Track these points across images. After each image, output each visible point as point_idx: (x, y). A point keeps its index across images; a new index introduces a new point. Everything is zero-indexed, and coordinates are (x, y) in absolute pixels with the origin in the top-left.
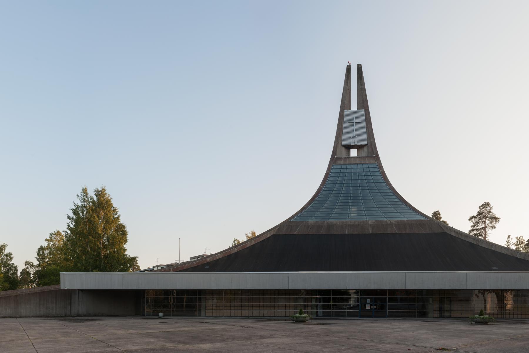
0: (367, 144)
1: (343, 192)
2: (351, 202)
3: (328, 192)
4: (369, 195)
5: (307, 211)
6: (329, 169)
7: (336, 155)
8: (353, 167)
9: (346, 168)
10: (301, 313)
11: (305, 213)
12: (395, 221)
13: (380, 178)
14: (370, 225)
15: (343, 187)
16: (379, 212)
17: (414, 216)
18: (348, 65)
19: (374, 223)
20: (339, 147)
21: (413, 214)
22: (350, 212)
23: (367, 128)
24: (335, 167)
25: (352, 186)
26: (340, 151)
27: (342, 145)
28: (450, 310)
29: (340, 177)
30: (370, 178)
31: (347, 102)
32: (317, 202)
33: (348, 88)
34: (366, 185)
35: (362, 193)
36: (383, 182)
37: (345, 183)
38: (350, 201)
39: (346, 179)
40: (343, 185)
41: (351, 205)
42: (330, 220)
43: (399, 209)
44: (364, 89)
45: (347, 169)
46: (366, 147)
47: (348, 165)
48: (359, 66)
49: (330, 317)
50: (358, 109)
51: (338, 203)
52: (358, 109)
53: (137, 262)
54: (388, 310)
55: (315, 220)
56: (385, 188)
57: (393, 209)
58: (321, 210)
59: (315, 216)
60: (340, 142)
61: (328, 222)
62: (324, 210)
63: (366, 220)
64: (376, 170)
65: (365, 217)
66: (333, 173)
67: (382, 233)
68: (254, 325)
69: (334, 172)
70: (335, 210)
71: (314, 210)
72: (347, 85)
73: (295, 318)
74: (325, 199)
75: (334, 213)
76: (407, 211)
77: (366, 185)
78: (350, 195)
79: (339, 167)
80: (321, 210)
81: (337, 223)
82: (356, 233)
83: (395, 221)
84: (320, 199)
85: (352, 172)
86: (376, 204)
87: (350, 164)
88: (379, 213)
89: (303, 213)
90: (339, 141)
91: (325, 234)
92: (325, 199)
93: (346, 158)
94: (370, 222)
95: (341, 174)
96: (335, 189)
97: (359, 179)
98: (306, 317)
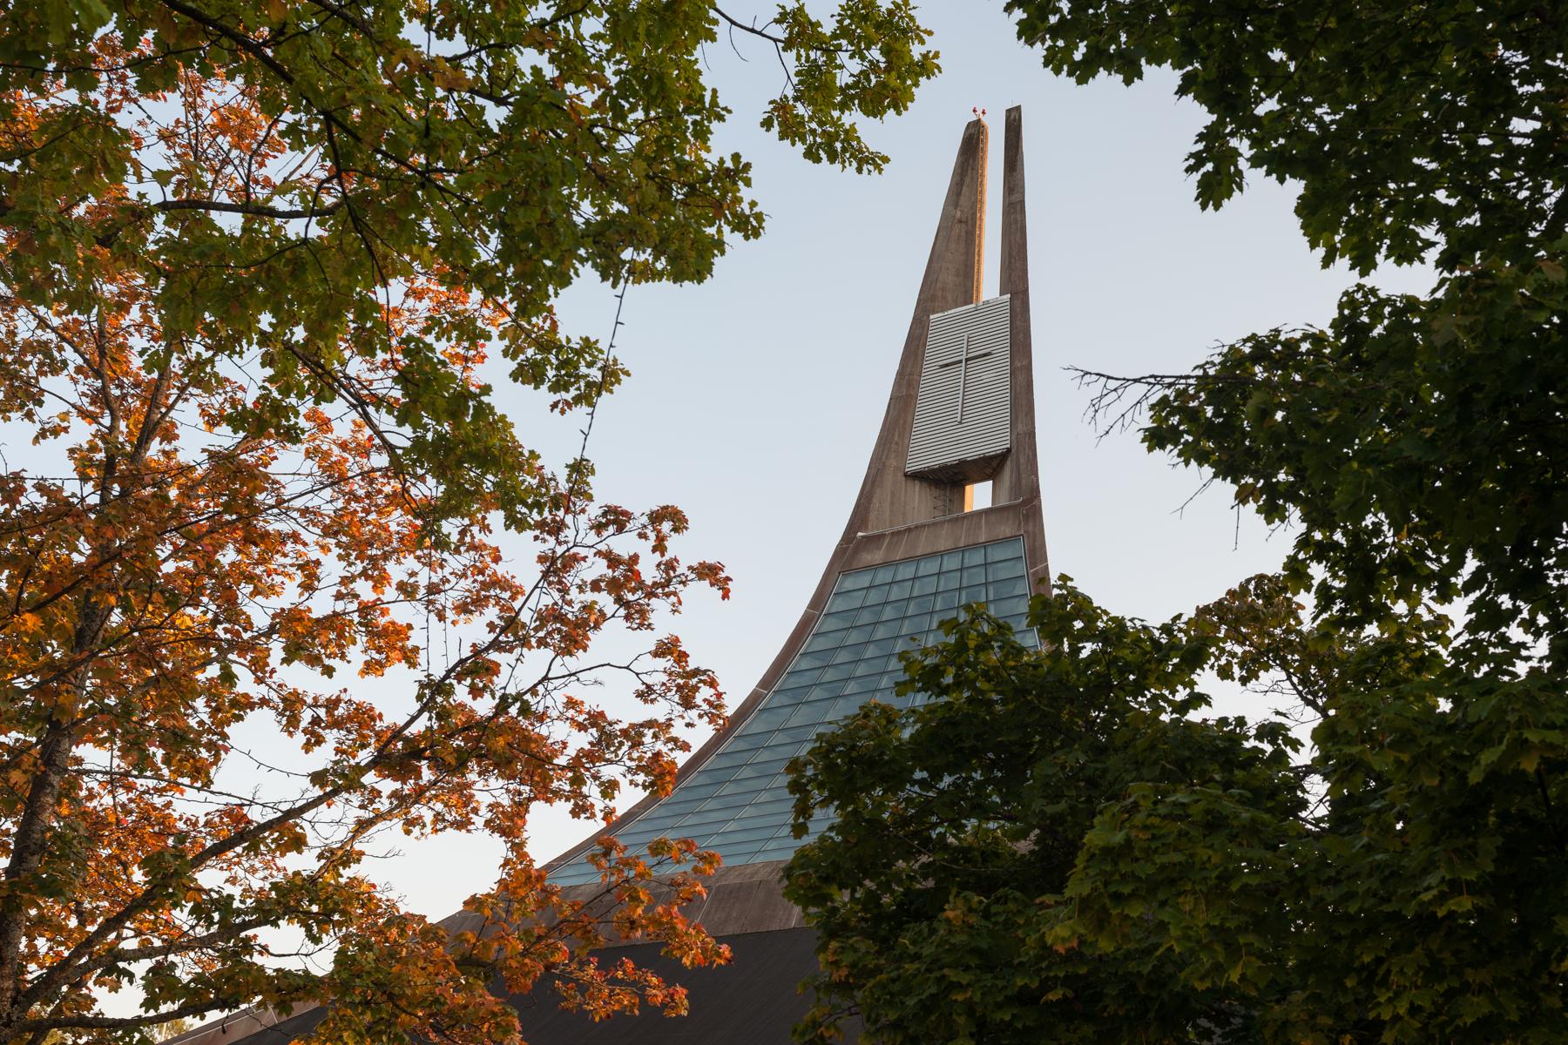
6: (818, 601)
24: (849, 584)
26: (892, 503)
27: (906, 475)
40: (966, 561)
53: (909, 104)
79: (865, 580)
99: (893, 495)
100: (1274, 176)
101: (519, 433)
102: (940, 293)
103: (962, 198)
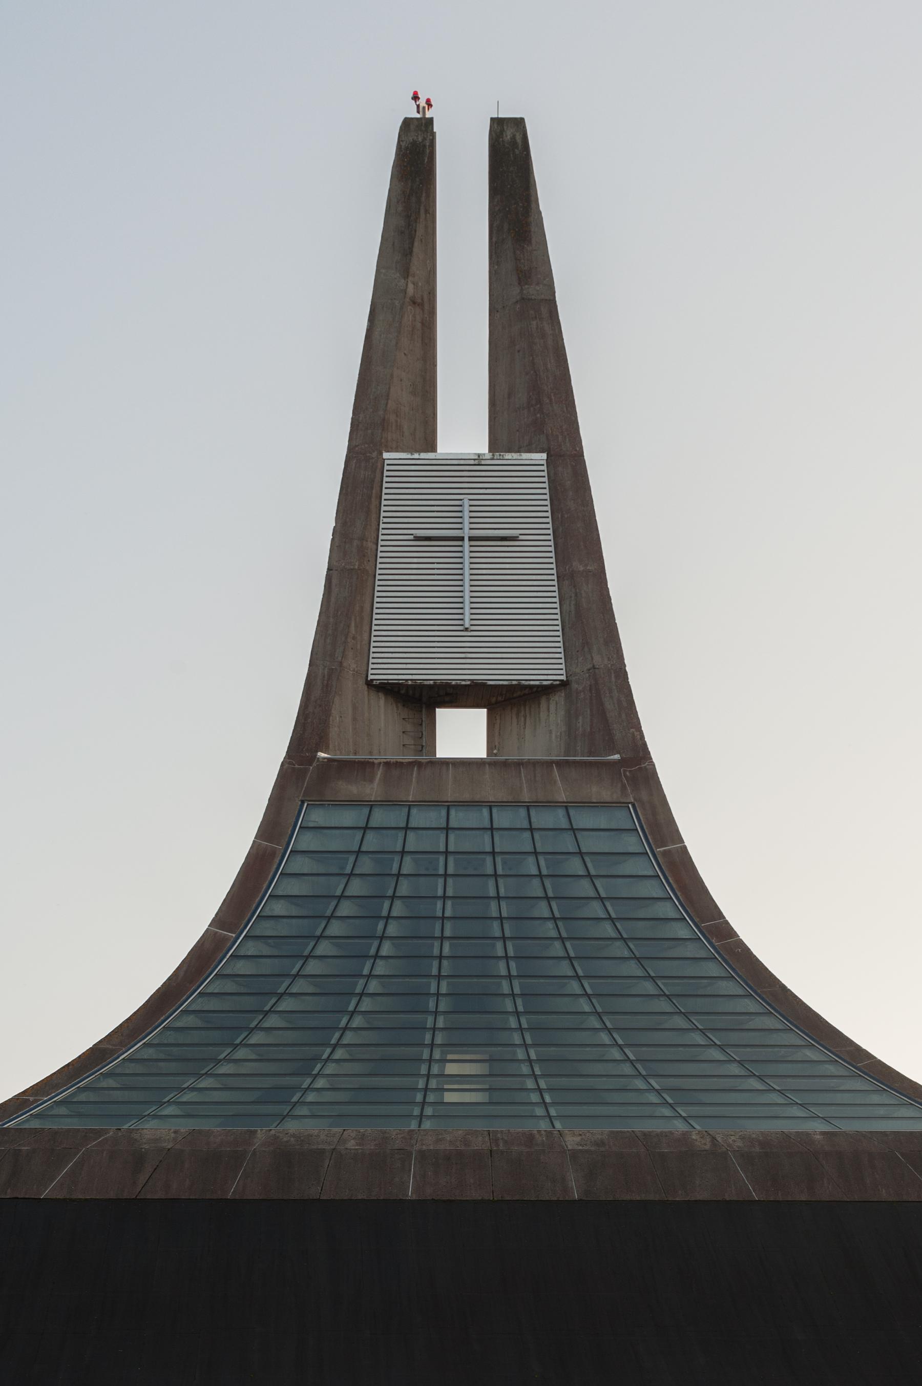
0: (564, 684)
3: (267, 966)
5: (118, 1071)
7: (323, 743)
8: (413, 824)
11: (111, 1083)
13: (657, 893)
14: (574, 1155)
16: (640, 1084)
17: (882, 1111)
18: (407, 123)
19: (601, 1143)
21: (876, 1098)
22: (437, 1055)
23: (565, 576)
24: (318, 817)
26: (354, 719)
27: (369, 684)
30: (584, 888)
33: (411, 289)
34: (549, 929)
35: (519, 976)
36: (672, 914)
37: (394, 913)
38: (437, 944)
41: (446, 951)
42: (292, 1126)
43: (783, 1069)
44: (544, 310)
46: (559, 699)
47: (414, 811)
48: (502, 131)
50: (494, 446)
51: (362, 994)
52: (491, 450)
55: (186, 1126)
56: (689, 955)
57: (735, 1069)
59: (184, 1099)
60: (351, 664)
63: (544, 1125)
64: (631, 843)
65: (540, 1111)
67: (651, 1197)
69: (312, 848)
72: (406, 273)
74: (248, 1002)
76: (833, 1083)
79: (349, 817)
83: (742, 1138)
84: (213, 1004)
86: (609, 1025)
88: (604, 1045)
89: (97, 1080)
91: (257, 1197)
92: (248, 1002)
93: (399, 765)
99: (355, 708)
102: (392, 418)
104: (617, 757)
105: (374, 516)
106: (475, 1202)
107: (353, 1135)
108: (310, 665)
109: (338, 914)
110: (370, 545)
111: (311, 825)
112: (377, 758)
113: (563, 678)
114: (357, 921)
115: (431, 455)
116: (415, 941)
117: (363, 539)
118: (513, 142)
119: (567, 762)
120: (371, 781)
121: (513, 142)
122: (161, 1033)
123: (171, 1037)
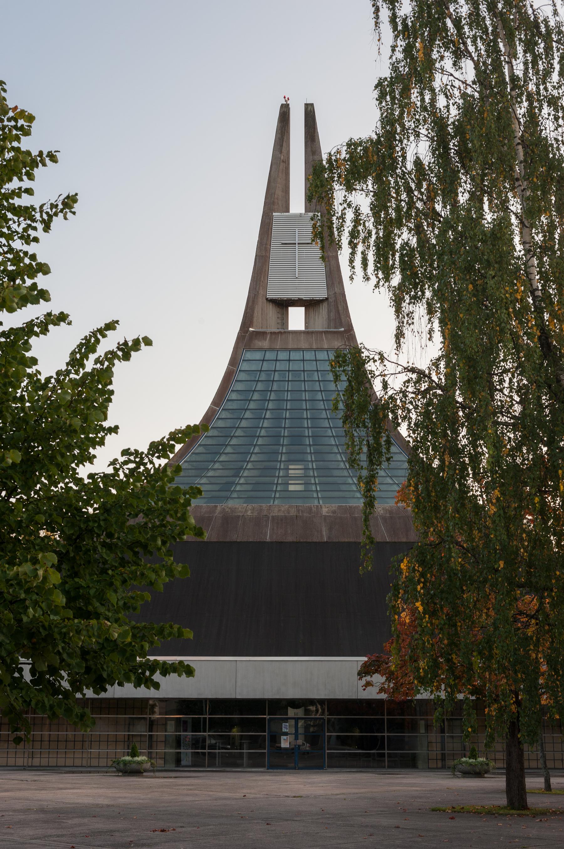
1: (265, 425)
2: (284, 451)
3: (229, 423)
4: (329, 433)
6: (234, 361)
7: (251, 325)
8: (291, 358)
9: (275, 359)
10: (134, 755)
12: (383, 509)
15: (267, 409)
18: (282, 105)
19: (334, 512)
20: (261, 302)
24: (249, 355)
25: (288, 407)
26: (262, 314)
27: (267, 299)
28: (131, 737)
29: (259, 384)
31: (279, 193)
32: (201, 449)
39: (275, 388)
42: (231, 504)
45: (278, 363)
46: (325, 304)
47: (279, 352)
49: (204, 766)
54: (328, 750)
58: (211, 473)
60: (261, 292)
61: (224, 509)
62: (218, 473)
66: (221, 419)
68: (42, 778)
70: (245, 475)
71: (192, 472)
72: (281, 152)
73: (122, 766)
75: (242, 481)
77: (323, 407)
78: (283, 432)
79: (258, 355)
80: (211, 473)
81: (246, 511)
82: (290, 539)
85: (289, 371)
87: (285, 349)
90: (261, 288)
91: (215, 540)
93: (275, 333)
94: (325, 511)
95: (263, 374)
96: (248, 415)
97: (305, 391)
98: (142, 763)
99: (262, 309)
100: (28, 354)
101: (156, 441)
102: (276, 201)
103: (283, 148)
104: (343, 329)
105: (270, 236)
106: (290, 542)
107: (250, 508)
108: (249, 293)
109: (253, 399)
110: (269, 246)
111: (246, 359)
112: (269, 330)
113: (326, 296)
114: (259, 402)
115: (287, 214)
116: (277, 411)
117: (266, 244)
118: (311, 111)
119: (327, 331)
120: (266, 340)
121: (311, 111)
122: (190, 456)
123: (194, 458)
